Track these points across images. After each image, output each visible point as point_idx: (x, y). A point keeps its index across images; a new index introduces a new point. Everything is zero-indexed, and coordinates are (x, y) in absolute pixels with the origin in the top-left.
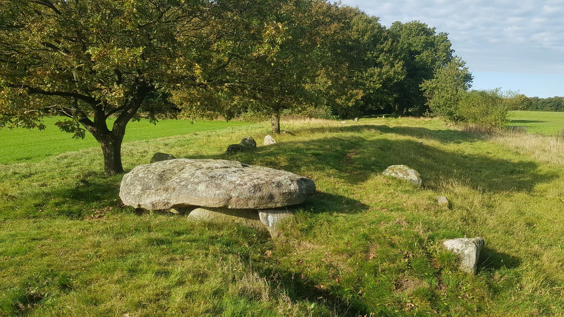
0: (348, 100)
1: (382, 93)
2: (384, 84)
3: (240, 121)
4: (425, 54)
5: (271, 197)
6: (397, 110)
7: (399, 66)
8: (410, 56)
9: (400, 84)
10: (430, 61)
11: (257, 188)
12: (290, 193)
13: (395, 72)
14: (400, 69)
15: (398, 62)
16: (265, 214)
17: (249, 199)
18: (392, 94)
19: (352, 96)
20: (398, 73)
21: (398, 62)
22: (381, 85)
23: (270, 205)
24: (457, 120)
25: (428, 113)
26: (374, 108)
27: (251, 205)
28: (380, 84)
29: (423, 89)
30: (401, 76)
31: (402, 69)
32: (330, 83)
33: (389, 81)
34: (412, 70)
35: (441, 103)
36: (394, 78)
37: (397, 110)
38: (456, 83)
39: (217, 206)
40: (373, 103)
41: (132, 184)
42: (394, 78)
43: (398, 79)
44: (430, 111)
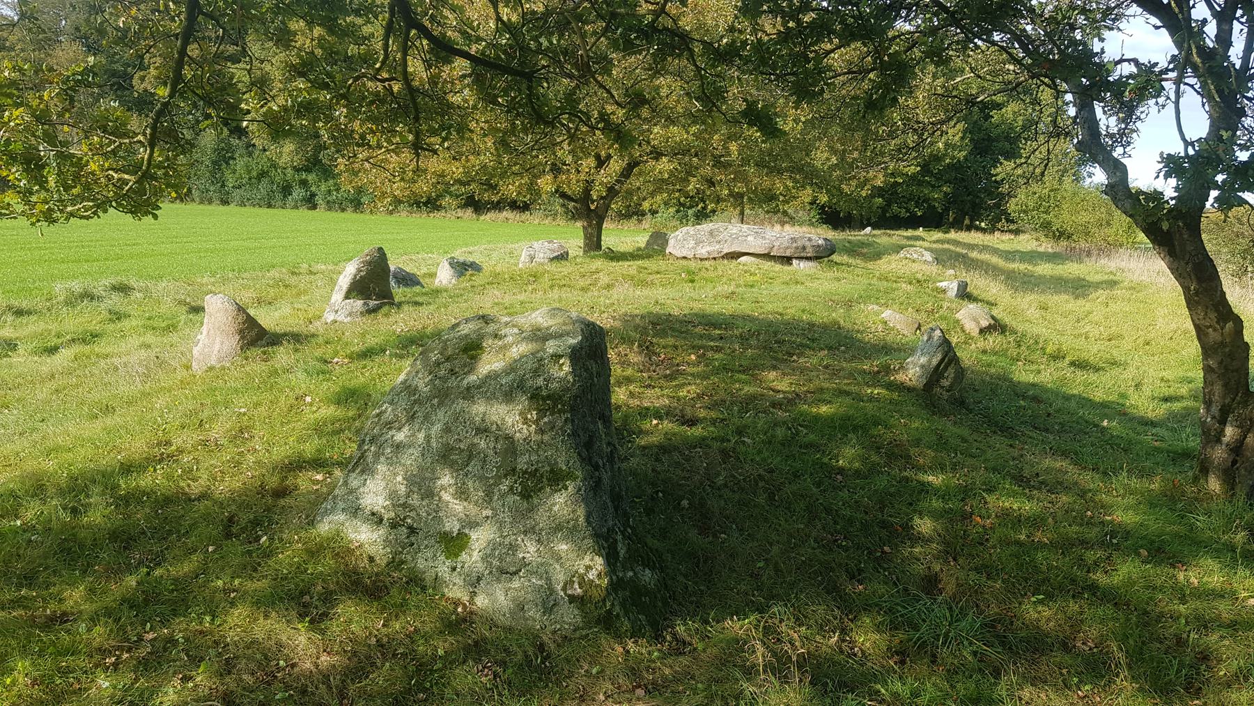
0: (862, 185)
1: (920, 183)
2: (925, 168)
3: (644, 229)
4: (1011, 109)
5: (804, 248)
6: (951, 220)
7: (955, 132)
8: (981, 112)
9: (956, 167)
10: (1020, 123)
11: (794, 240)
12: (819, 246)
13: (947, 145)
14: (957, 138)
15: (955, 124)
16: (798, 262)
17: (787, 248)
18: (939, 186)
19: (867, 181)
20: (954, 147)
21: (955, 124)
22: (919, 168)
23: (802, 255)
24: (1059, 237)
25: (1005, 224)
26: (904, 214)
27: (788, 254)
28: (917, 166)
29: (999, 178)
30: (960, 151)
31: (962, 138)
32: (834, 160)
33: (934, 160)
34: (983, 139)
35: (1031, 204)
36: (945, 155)
37: (951, 220)
38: (1062, 167)
39: (762, 253)
40: (901, 203)
41: (684, 240)
42: (945, 155)
43: (953, 158)
44: (1008, 220)
